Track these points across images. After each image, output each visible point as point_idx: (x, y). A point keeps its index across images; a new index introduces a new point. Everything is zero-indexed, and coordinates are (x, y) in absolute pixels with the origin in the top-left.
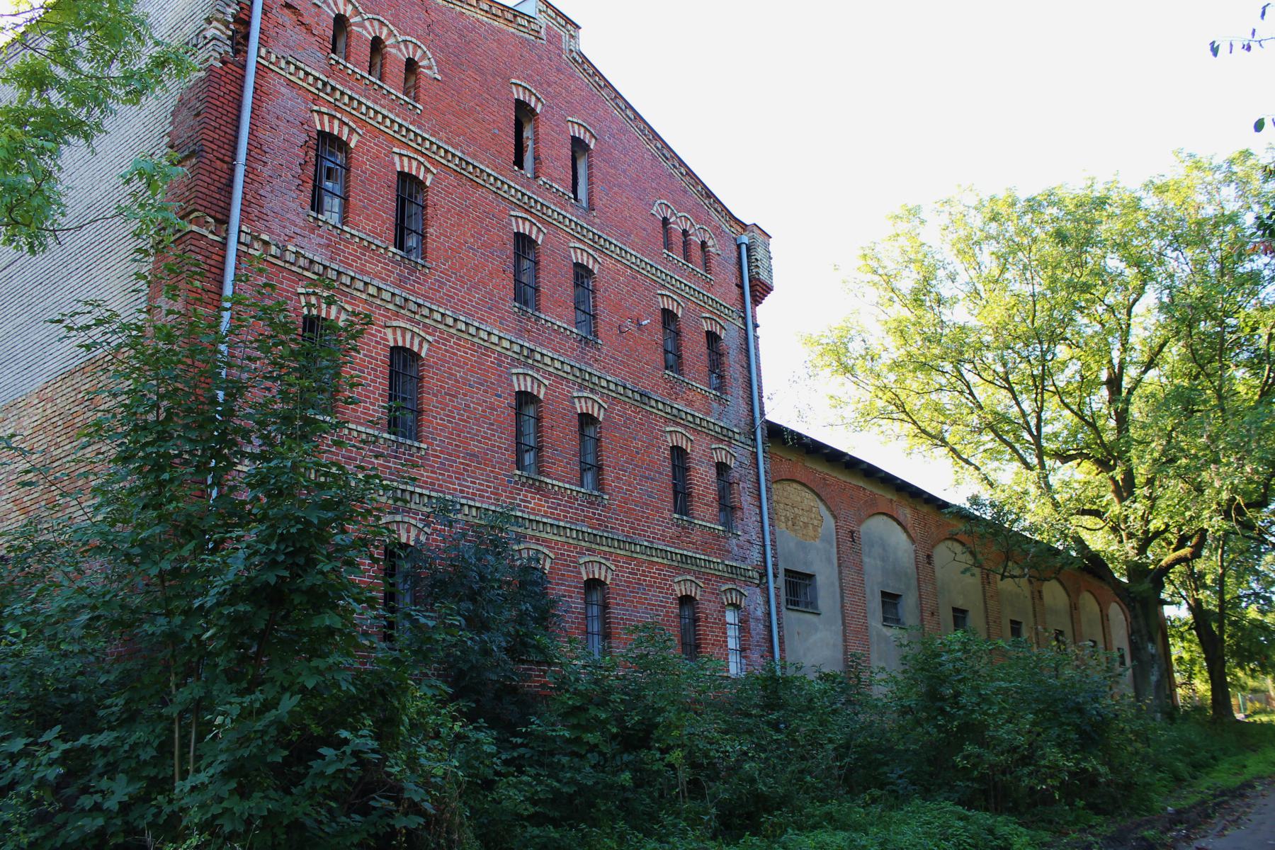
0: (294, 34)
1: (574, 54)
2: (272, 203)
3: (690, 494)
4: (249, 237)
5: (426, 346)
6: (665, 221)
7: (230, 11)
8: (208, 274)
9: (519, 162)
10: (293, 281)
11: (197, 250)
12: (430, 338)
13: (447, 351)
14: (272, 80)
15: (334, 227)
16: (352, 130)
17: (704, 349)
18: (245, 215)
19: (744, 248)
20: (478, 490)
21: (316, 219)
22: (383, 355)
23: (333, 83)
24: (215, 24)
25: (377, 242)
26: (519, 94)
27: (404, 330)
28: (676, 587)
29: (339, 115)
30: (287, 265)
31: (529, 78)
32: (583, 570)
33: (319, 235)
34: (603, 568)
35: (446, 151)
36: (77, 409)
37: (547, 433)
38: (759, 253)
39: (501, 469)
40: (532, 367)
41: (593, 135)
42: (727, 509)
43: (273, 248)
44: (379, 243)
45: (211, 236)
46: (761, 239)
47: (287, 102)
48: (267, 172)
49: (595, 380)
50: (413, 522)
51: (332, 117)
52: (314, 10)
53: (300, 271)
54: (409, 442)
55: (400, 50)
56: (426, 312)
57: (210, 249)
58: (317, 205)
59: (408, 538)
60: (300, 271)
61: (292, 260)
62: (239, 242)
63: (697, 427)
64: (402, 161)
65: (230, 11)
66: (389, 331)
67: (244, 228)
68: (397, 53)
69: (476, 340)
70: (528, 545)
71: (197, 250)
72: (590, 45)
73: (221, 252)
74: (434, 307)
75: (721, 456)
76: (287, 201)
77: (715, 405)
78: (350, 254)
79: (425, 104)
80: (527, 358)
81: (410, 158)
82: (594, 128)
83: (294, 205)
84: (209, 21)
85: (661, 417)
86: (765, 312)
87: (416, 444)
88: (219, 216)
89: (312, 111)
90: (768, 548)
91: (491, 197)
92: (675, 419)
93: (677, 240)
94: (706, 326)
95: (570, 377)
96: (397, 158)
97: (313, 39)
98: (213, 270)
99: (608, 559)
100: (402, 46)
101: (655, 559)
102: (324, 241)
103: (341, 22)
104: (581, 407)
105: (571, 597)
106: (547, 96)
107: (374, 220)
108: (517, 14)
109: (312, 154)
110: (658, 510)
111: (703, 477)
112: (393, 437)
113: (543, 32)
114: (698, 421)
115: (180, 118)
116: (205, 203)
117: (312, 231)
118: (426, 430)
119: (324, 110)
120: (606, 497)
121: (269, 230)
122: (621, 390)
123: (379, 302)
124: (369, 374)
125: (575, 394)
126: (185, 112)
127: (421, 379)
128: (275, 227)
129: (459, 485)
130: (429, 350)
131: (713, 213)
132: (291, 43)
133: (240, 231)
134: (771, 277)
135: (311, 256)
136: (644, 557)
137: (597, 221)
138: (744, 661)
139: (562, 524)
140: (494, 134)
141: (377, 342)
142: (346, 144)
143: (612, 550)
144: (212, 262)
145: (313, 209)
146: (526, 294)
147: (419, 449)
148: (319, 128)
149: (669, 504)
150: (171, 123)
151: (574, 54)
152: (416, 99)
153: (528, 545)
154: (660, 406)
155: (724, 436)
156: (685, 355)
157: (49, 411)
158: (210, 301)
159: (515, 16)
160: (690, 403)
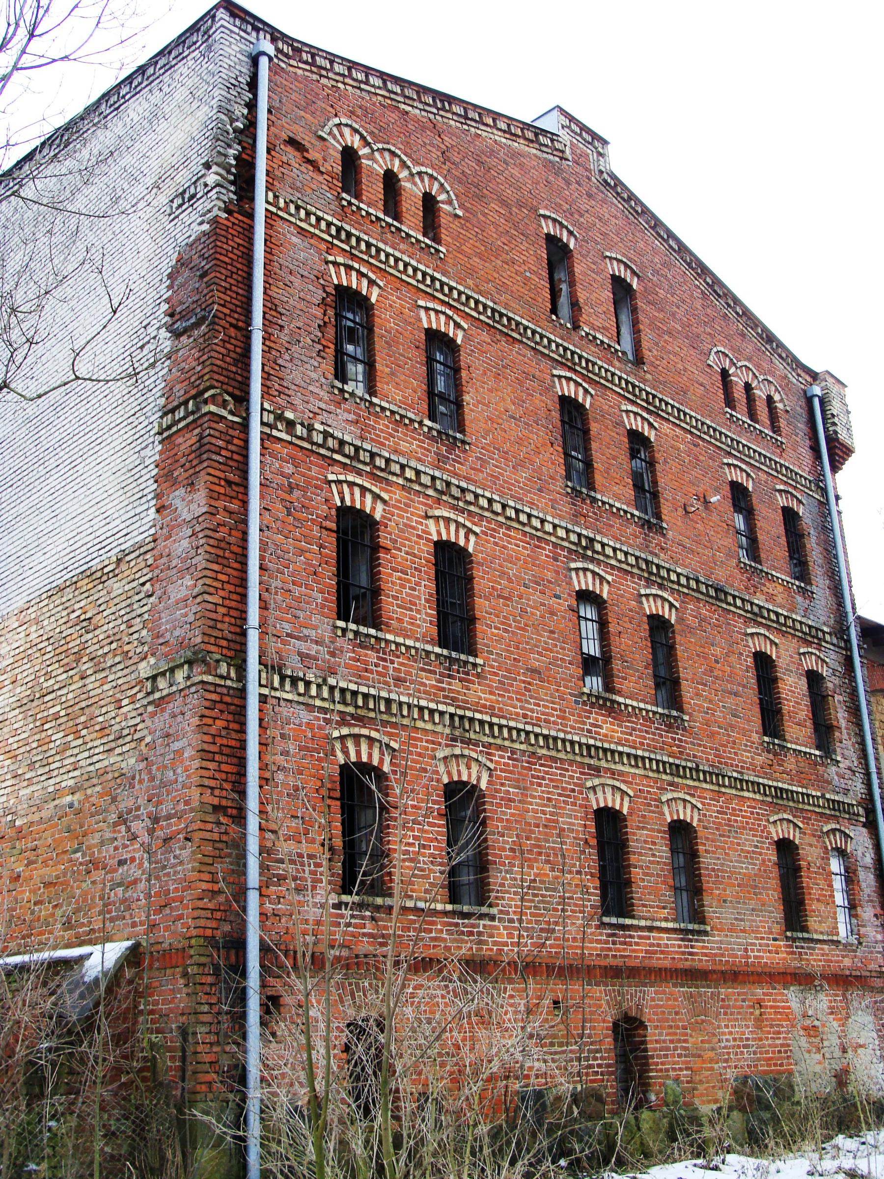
0: (300, 173)
1: (605, 176)
2: (294, 375)
3: (779, 711)
4: (272, 416)
5: (472, 538)
6: (724, 373)
7: (231, 152)
8: (231, 463)
9: (554, 310)
10: (321, 467)
11: (217, 434)
12: (477, 529)
13: (496, 544)
14: (279, 225)
15: (361, 399)
16: (371, 283)
17: (781, 530)
18: (266, 392)
19: (816, 402)
20: (543, 714)
21: (342, 391)
22: (426, 551)
23: (347, 227)
24: (215, 168)
25: (410, 415)
26: (548, 228)
27: (447, 520)
28: (772, 829)
29: (356, 266)
30: (314, 448)
31: (557, 208)
32: (666, 809)
33: (346, 410)
34: (689, 806)
35: (477, 302)
36: (70, 631)
37: (614, 640)
38: (835, 408)
39: (566, 687)
40: (592, 560)
41: (634, 273)
42: (824, 732)
43: (299, 427)
44: (413, 417)
45: (230, 417)
46: (835, 389)
47: (300, 253)
48: (284, 337)
49: (664, 573)
50: (474, 755)
51: (349, 268)
52: (318, 143)
53: (328, 454)
54: (463, 657)
55: (415, 184)
56: (470, 497)
57: (231, 432)
58: (341, 374)
59: (470, 775)
60: (328, 454)
61: (320, 441)
62: (263, 423)
63: (782, 626)
64: (429, 318)
65: (231, 152)
66: (431, 522)
67: (266, 406)
68: (412, 190)
69: (527, 529)
70: (602, 781)
71: (217, 434)
72: (621, 162)
73: (242, 436)
74: (480, 491)
75: (810, 663)
76: (309, 372)
77: (799, 599)
78: (382, 431)
79: (447, 245)
80: (585, 549)
81: (437, 312)
82: (635, 262)
83: (314, 375)
84: (207, 166)
85: (740, 616)
86: (845, 481)
87: (471, 659)
88: (237, 393)
89: (327, 262)
90: (874, 777)
91: (529, 354)
92: (756, 616)
93: (739, 394)
94: (782, 501)
95: (635, 571)
96: (422, 313)
97: (321, 178)
98: (236, 457)
99: (693, 796)
100: (417, 179)
101: (746, 794)
102: (352, 417)
103: (349, 156)
104: (650, 607)
105: (654, 843)
106: (580, 226)
107: (403, 386)
108: (539, 132)
109: (331, 312)
110: (744, 732)
111: (792, 690)
112: (445, 652)
113: (568, 151)
114: (782, 620)
115: (180, 280)
116: (222, 378)
117: (338, 404)
118: (481, 641)
119: (340, 260)
120: (686, 718)
121: (292, 406)
122: (693, 584)
123: (417, 487)
124: (413, 576)
125: (643, 592)
126: (187, 273)
127: (470, 579)
128: (297, 401)
129: (522, 708)
130: (476, 543)
131: (777, 361)
132: (299, 184)
133: (263, 409)
134: (851, 436)
135: (340, 436)
136: (734, 792)
137: (648, 376)
138: (854, 921)
139: (640, 753)
140: (526, 278)
141: (419, 536)
142: (367, 299)
143: (696, 784)
144: (233, 448)
145: (336, 378)
146: (581, 474)
147: (475, 665)
148: (336, 282)
149: (756, 723)
150: (169, 287)
151: (605, 176)
152: (439, 242)
153: (602, 781)
154: (739, 603)
155: (811, 637)
156: (761, 537)
157: (34, 636)
158: (234, 494)
159: (536, 135)
160: (770, 598)
